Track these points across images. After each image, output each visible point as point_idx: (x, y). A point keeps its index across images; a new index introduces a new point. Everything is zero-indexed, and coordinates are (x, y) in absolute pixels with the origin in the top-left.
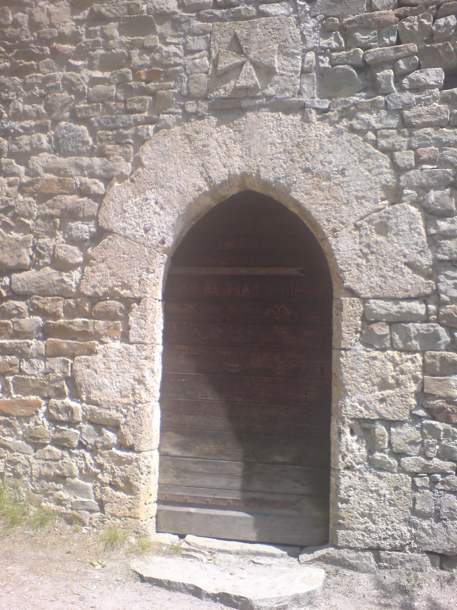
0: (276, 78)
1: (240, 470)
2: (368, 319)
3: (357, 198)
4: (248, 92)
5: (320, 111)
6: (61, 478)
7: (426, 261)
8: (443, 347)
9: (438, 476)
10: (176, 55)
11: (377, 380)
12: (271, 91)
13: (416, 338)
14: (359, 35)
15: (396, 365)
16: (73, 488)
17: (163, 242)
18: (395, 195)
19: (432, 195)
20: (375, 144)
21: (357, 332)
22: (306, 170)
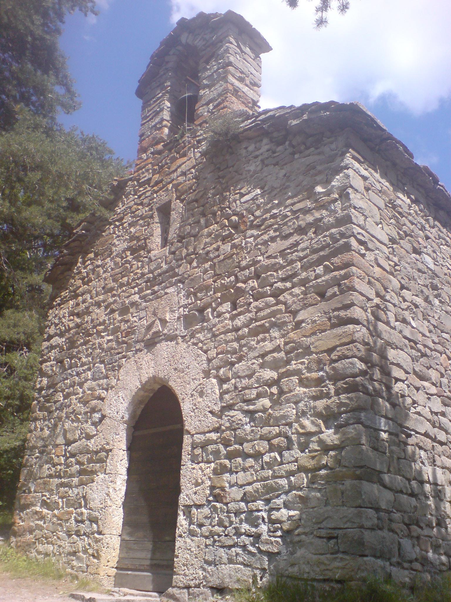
0: (168, 324)
1: (151, 546)
2: (194, 446)
3: (193, 379)
4: (157, 333)
5: (183, 337)
6: (74, 553)
7: (217, 408)
8: (222, 457)
9: (216, 537)
10: (135, 321)
11: (194, 481)
12: (166, 331)
13: (211, 453)
14: (199, 294)
15: (203, 471)
16: (79, 559)
17: (123, 418)
18: (207, 374)
19: (222, 371)
20: (201, 349)
21: (189, 455)
22: (175, 369)
